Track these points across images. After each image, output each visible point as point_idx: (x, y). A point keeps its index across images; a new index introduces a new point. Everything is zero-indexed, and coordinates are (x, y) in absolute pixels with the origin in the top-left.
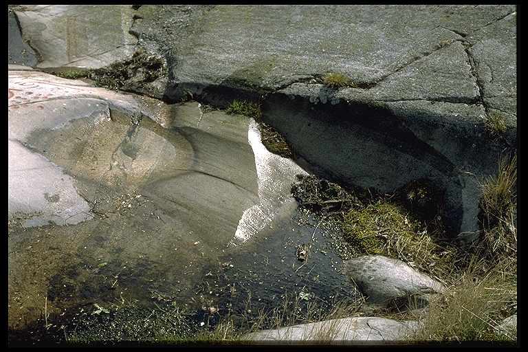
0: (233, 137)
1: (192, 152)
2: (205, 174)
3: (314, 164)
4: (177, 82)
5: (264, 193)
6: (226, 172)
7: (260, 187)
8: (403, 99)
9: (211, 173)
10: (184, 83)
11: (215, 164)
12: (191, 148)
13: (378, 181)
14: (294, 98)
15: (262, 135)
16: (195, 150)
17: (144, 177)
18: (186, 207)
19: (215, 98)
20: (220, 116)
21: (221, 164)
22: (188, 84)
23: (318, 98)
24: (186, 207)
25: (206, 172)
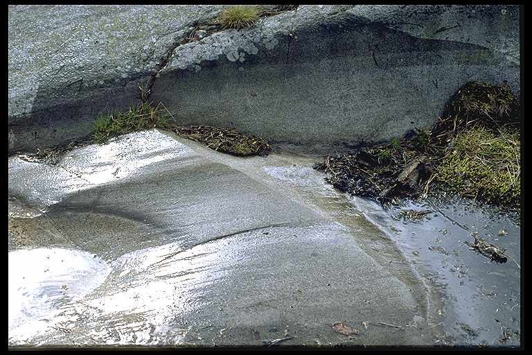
3: (310, 143)
13: (408, 119)
14: (198, 68)
23: (240, 51)
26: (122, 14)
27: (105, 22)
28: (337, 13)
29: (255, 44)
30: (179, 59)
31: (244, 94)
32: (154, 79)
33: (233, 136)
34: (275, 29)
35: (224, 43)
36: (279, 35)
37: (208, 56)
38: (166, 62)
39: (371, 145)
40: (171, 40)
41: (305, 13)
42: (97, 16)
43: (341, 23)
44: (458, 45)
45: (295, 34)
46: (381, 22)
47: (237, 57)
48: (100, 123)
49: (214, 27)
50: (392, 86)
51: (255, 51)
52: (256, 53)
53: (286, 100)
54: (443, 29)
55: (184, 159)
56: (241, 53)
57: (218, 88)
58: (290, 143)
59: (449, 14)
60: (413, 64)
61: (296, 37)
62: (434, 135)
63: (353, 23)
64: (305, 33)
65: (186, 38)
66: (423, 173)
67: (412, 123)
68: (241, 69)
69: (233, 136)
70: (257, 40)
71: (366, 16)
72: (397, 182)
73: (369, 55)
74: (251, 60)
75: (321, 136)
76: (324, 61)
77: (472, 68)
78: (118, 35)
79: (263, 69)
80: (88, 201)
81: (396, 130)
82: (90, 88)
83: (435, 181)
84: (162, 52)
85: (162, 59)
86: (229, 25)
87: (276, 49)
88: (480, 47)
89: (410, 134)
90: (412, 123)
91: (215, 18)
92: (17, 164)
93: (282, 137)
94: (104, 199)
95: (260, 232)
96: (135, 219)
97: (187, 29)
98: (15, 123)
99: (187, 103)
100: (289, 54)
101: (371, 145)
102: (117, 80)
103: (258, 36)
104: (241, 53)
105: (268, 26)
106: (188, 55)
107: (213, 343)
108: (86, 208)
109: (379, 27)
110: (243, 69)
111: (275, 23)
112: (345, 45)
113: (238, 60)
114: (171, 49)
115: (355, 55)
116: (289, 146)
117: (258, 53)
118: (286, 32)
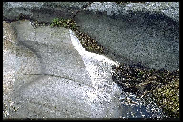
0: (62, 45)
1: (37, 59)
2: (53, 76)
3: (119, 56)
4: (10, 8)
5: (97, 85)
6: (67, 72)
7: (93, 81)
8: (172, 8)
9: (56, 75)
10: (15, 8)
11: (61, 68)
12: (36, 56)
13: (165, 64)
14: (95, 13)
15: (80, 39)
16: (39, 57)
17: (11, 85)
18: (49, 107)
19: (39, 17)
20: (48, 30)
21: (63, 68)
22: (18, 8)
23: (112, 12)
24: (49, 107)
25: (52, 74)
28: (157, 10)
29: (119, 11)
30: (91, 7)
31: (106, 28)
32: (79, 11)
33: (93, 42)
37: (101, 10)
38: (87, 6)
39: (143, 68)
46: (173, 20)
56: (112, 13)
57: (98, 23)
61: (135, 14)
62: (170, 75)
63: (161, 16)
66: (149, 87)
67: (166, 66)
68: (110, 19)
69: (93, 42)
70: (120, 10)
71: (168, 16)
73: (163, 32)
74: (114, 17)
75: (125, 55)
76: (142, 27)
79: (118, 22)
80: (30, 44)
81: (158, 66)
82: (59, 7)
83: (151, 93)
85: (86, 5)
87: (126, 16)
89: (162, 70)
90: (166, 66)
93: (110, 50)
94: (35, 46)
98: (35, 10)
99: (85, 24)
101: (143, 68)
102: (68, 7)
104: (112, 13)
105: (128, 6)
107: (109, 118)
112: (154, 24)
115: (157, 30)
116: (111, 54)
117: (118, 15)
118: (133, 10)
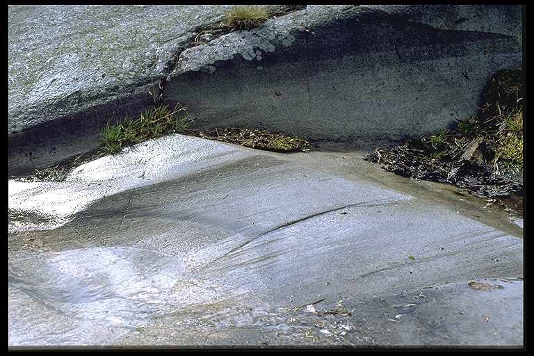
13: (446, 112)
14: (212, 69)
23: (255, 49)
26: (109, 29)
27: (92, 38)
34: (289, 26)
35: (234, 44)
36: (295, 32)
37: (221, 56)
40: (175, 45)
41: (313, 14)
42: (81, 33)
43: (357, 17)
44: (481, 36)
45: (312, 30)
47: (254, 56)
48: (109, 133)
49: (220, 30)
50: (421, 79)
51: (272, 48)
52: (274, 50)
53: (314, 98)
54: (463, 20)
55: (222, 155)
58: (329, 140)
59: (463, 10)
60: (438, 57)
61: (313, 33)
64: (323, 29)
65: (191, 43)
68: (260, 68)
72: (464, 161)
77: (499, 58)
78: (111, 47)
80: (118, 206)
83: (501, 159)
84: (169, 56)
86: (240, 25)
88: (503, 36)
90: (452, 115)
91: (219, 22)
92: (14, 186)
95: (337, 213)
96: (181, 219)
97: (190, 35)
100: (306, 54)
103: (272, 33)
106: (197, 58)
108: (118, 213)
109: (393, 18)
110: (261, 68)
111: (285, 23)
113: (255, 58)
114: (178, 53)
115: (377, 50)
116: (329, 143)
117: (276, 51)
